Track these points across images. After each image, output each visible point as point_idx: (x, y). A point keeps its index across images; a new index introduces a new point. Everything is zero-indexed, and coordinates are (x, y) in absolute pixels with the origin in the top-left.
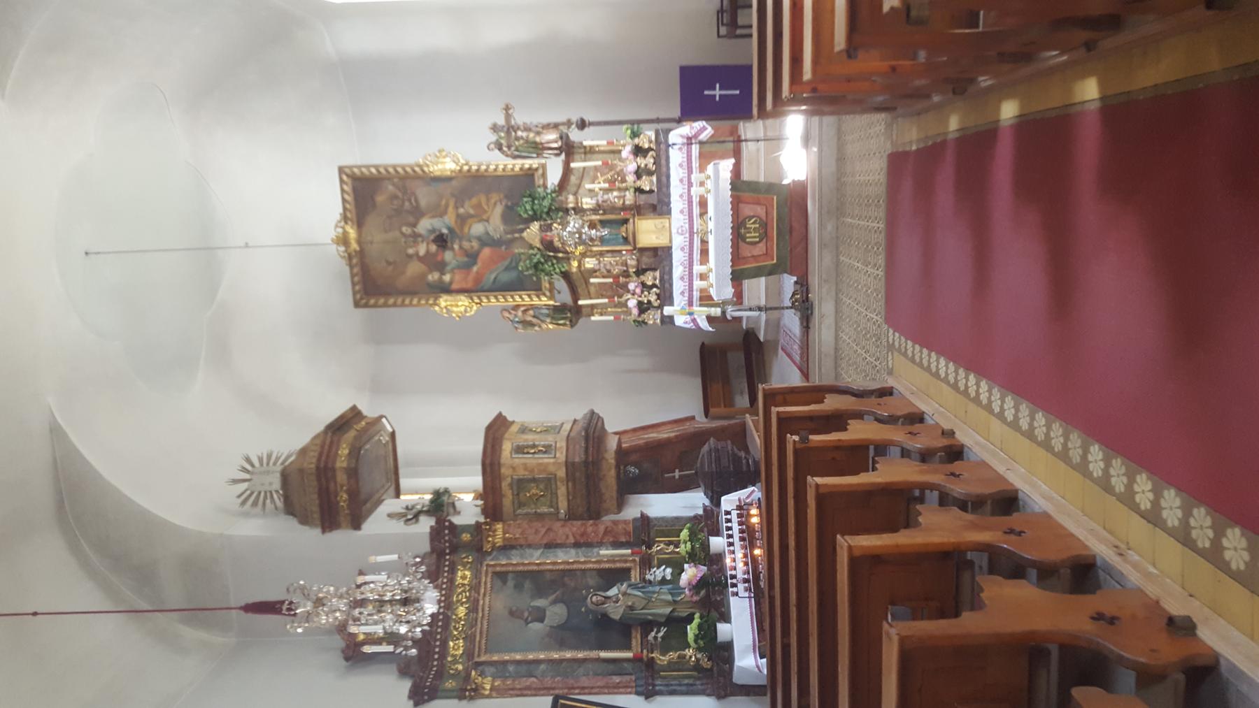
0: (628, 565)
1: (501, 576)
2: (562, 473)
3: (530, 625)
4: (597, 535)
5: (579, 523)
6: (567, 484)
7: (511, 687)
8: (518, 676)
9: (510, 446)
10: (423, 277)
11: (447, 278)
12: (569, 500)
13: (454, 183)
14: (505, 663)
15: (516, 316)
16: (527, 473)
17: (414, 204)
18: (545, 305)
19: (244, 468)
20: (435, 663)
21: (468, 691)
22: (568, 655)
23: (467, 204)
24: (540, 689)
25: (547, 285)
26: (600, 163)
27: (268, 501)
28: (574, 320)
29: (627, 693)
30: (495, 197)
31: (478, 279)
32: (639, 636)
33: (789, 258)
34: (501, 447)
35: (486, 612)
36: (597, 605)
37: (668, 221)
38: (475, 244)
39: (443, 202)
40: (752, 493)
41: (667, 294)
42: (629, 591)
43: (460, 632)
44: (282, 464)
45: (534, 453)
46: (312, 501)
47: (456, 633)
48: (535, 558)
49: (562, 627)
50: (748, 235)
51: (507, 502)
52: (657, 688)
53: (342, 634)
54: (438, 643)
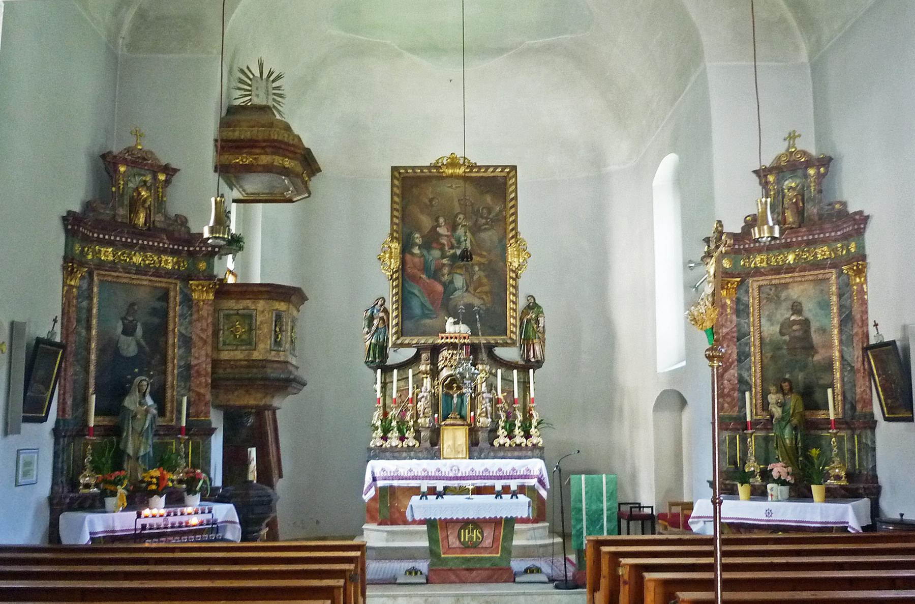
0: (168, 414)
1: (165, 296)
2: (256, 355)
3: (120, 322)
4: (197, 387)
5: (209, 370)
6: (244, 360)
8: (79, 309)
9: (282, 309)
10: (419, 230)
11: (416, 251)
12: (230, 361)
13: (501, 264)
14: (90, 299)
15: (378, 311)
16: (258, 323)
18: (388, 339)
19: (273, 73)
20: (96, 235)
21: (71, 264)
22: (93, 357)
23: (482, 274)
24: (67, 330)
25: (407, 342)
26: (516, 396)
27: (243, 93)
28: (372, 365)
31: (416, 279)
32: (106, 423)
33: (445, 568)
34: (283, 301)
35: (135, 282)
36: (138, 385)
37: (464, 456)
38: (446, 278)
39: (484, 253)
40: (233, 534)
41: (396, 454)
42: (149, 417)
43: (119, 257)
44: (274, 106)
45: (276, 331)
46: (243, 133)
47: (119, 253)
48: (176, 327)
50: (467, 531)
51: (231, 304)
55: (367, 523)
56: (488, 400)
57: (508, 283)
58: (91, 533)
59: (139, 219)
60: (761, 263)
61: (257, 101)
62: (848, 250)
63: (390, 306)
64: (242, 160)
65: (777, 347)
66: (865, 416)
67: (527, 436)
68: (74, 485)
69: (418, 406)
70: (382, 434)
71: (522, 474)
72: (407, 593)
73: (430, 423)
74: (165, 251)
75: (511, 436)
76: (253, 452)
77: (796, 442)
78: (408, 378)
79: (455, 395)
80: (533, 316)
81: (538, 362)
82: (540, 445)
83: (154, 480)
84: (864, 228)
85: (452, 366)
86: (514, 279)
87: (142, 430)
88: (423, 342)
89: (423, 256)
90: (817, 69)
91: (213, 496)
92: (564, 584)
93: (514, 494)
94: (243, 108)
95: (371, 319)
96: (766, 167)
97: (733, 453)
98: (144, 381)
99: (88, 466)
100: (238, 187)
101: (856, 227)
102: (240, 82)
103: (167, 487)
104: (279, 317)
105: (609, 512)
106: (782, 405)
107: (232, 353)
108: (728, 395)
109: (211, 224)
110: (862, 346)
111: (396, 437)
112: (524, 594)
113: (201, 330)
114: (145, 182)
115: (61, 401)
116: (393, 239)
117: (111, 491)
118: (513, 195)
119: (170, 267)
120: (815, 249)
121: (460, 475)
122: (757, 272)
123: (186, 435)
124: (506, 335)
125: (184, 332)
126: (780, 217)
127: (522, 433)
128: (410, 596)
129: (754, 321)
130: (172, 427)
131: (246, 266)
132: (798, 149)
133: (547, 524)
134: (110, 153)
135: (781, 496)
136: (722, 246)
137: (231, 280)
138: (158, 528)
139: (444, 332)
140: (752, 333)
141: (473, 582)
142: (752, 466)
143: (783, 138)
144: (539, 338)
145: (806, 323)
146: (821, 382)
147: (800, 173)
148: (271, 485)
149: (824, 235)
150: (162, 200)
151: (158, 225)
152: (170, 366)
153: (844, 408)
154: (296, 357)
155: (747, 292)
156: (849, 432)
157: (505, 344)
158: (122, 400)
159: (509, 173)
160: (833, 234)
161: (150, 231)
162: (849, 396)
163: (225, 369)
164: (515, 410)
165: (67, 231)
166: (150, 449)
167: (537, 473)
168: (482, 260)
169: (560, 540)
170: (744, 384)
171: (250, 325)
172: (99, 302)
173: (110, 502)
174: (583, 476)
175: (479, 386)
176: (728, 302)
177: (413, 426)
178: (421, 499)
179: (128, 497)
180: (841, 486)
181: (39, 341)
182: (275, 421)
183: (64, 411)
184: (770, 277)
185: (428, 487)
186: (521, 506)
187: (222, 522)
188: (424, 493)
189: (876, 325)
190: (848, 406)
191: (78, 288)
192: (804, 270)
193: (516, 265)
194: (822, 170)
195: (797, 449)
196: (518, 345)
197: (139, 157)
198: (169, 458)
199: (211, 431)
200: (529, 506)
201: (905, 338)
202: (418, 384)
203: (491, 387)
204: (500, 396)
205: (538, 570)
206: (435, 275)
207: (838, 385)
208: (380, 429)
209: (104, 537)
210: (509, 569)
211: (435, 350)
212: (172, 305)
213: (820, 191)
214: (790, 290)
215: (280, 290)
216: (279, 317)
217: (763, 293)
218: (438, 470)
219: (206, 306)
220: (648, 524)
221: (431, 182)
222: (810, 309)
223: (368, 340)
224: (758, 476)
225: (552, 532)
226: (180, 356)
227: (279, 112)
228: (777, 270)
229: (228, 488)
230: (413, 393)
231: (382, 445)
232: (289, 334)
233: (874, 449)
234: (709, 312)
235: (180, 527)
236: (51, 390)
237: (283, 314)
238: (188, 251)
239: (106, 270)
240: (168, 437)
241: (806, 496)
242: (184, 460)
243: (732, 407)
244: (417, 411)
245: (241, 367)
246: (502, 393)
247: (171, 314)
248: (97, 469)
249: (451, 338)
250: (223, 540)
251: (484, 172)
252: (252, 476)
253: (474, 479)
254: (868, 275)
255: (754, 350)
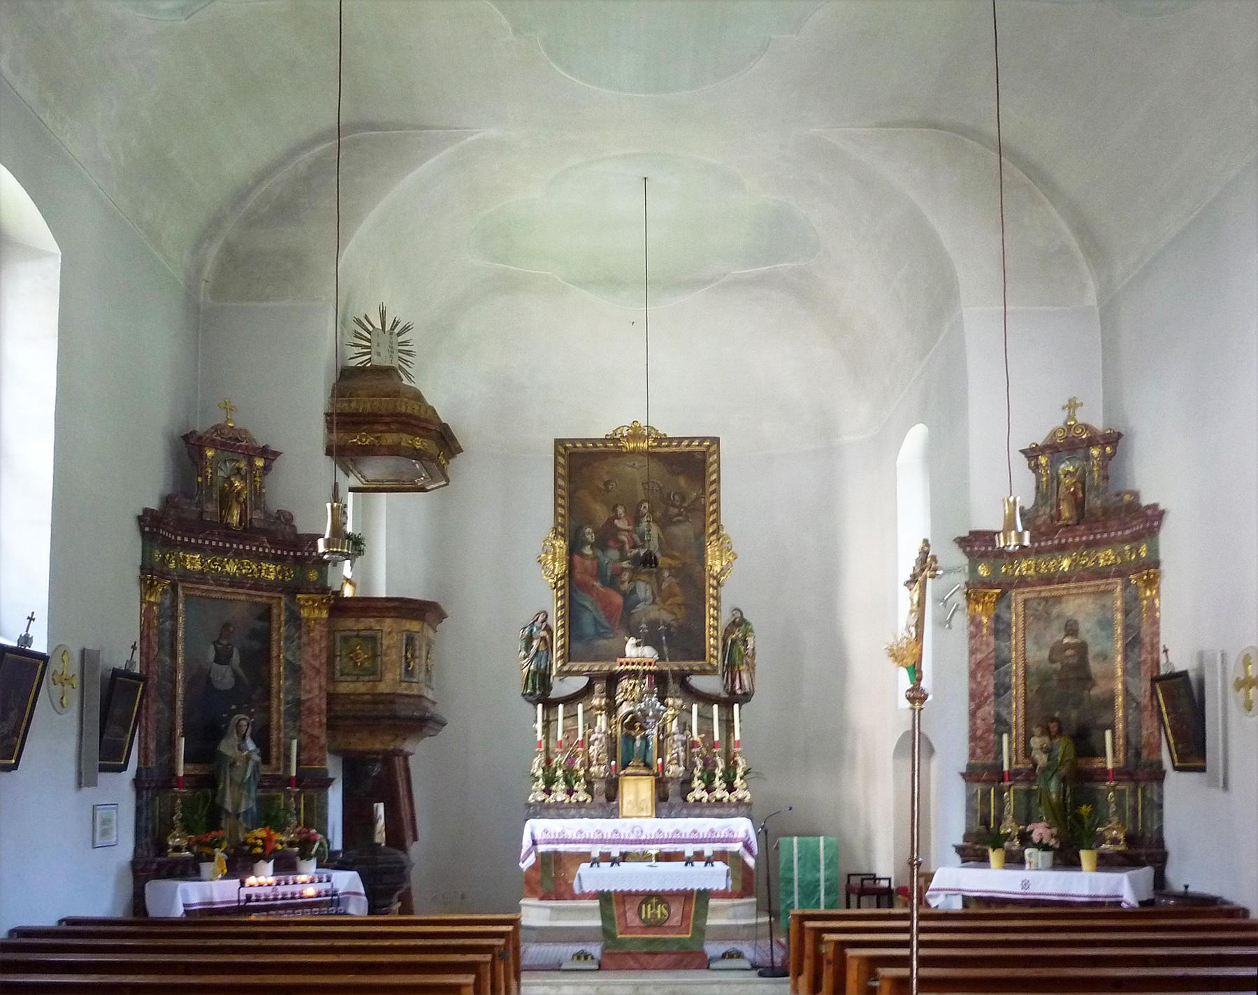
0: (274, 762)
1: (266, 614)
2: (383, 688)
3: (212, 647)
5: (324, 706)
7: (152, 626)
8: (161, 632)
9: (415, 630)
10: (590, 522)
11: (588, 551)
14: (174, 617)
16: (384, 647)
17: (675, 519)
18: (551, 665)
19: (398, 323)
20: (179, 538)
21: (150, 574)
22: (180, 690)
25: (575, 669)
26: (717, 738)
28: (531, 698)
29: (139, 757)
30: (680, 613)
32: (197, 772)
35: (229, 597)
37: (649, 814)
38: (626, 587)
39: (677, 554)
40: (358, 908)
46: (363, 404)
48: (281, 653)
49: (209, 681)
50: (649, 906)
51: (350, 624)
52: (145, 792)
53: (213, 430)
54: (200, 542)
55: (526, 897)
56: (680, 743)
57: (707, 592)
58: (185, 905)
59: (232, 517)
60: (1027, 570)
61: (378, 361)
62: (1138, 555)
63: (554, 623)
64: (360, 440)
65: (1045, 678)
66: (1151, 765)
67: (731, 789)
68: (161, 847)
69: (591, 750)
70: (544, 787)
71: (722, 836)
72: (574, 981)
73: (605, 773)
74: (266, 558)
75: (709, 789)
76: (380, 809)
77: (1064, 796)
78: (577, 715)
79: (638, 737)
80: (740, 635)
81: (745, 694)
82: (747, 800)
83: (260, 842)
84: (1159, 527)
85: (633, 700)
86: (715, 588)
87: (242, 780)
88: (596, 669)
89: (596, 557)
90: (1108, 313)
91: (331, 862)
92: (769, 971)
93: (709, 861)
94: (361, 371)
95: (529, 640)
96: (1037, 445)
97: (986, 811)
98: (242, 719)
99: (179, 824)
100: (356, 472)
101: (1148, 525)
102: (356, 337)
103: (276, 850)
104: (410, 641)
105: (828, 883)
106: (1048, 751)
107: (352, 686)
108: (981, 738)
109: (327, 536)
110: (1152, 676)
111: (562, 790)
112: (719, 983)
113: (312, 656)
114: (239, 470)
115: (142, 746)
116: (557, 534)
117: (208, 855)
118: (714, 477)
119: (272, 577)
120: (1096, 552)
121: (643, 837)
122: (1023, 582)
123: (297, 786)
124: (704, 659)
125: (291, 659)
126: (1054, 511)
127: (724, 786)
128: (578, 985)
129: (1016, 644)
130: (278, 778)
131: (366, 576)
132: (1080, 421)
133: (754, 900)
134: (194, 432)
135: (1043, 864)
136: (927, 569)
137: (348, 592)
138: (266, 900)
139: (624, 656)
140: (1013, 660)
141: (657, 968)
142: (1008, 827)
143: (1060, 407)
144: (747, 664)
145: (1082, 648)
146: (1100, 722)
147: (1081, 453)
148: (404, 849)
149: (1109, 535)
150: (261, 493)
151: (256, 524)
152: (275, 702)
153: (1126, 754)
154: (433, 689)
155: (1009, 607)
156: (1132, 785)
157: (703, 672)
158: (218, 744)
159: (708, 447)
160: (1120, 533)
161: (247, 532)
162: (1133, 740)
163: (343, 705)
164: (715, 756)
165: (143, 534)
166: (252, 804)
167: (741, 835)
168: (673, 563)
169: (766, 919)
170: (1001, 724)
171: (374, 649)
172: (186, 623)
173: (206, 868)
174: (795, 839)
175: (668, 725)
176: (985, 620)
177: (584, 776)
178: (591, 866)
179: (227, 862)
180: (1119, 853)
181: (116, 672)
182: (407, 770)
183: (146, 757)
184: (1038, 588)
185: (600, 853)
186: (716, 877)
187: (343, 894)
188: (595, 859)
189: (1166, 651)
190: (1131, 752)
191: (159, 605)
192: (1081, 579)
193: (717, 569)
194: (1108, 449)
195: (1065, 804)
196: (720, 672)
197: (230, 438)
198: (276, 816)
199: (328, 782)
200: (727, 876)
201: (1200, 670)
202: (590, 723)
203: (685, 727)
204: (696, 737)
205: (739, 955)
206: (612, 582)
207: (1120, 726)
208: (541, 780)
209: (200, 910)
210: (702, 954)
211: (612, 680)
212: (275, 625)
213: (1106, 478)
214: (1064, 605)
215: (411, 606)
216: (410, 641)
217: (1029, 608)
218: (616, 832)
219: (317, 627)
220: (885, 899)
221: (607, 459)
222: (1088, 629)
223: (527, 667)
224: (1016, 839)
225: (759, 911)
226: (287, 689)
227: (407, 374)
228: (1048, 580)
229: (350, 852)
230: (584, 735)
231: (544, 800)
232: (423, 661)
233: (1161, 806)
234: (911, 646)
235: (293, 898)
236: (130, 733)
237: (416, 636)
238: (295, 555)
239: (193, 583)
240: (274, 790)
241: (1074, 864)
242: (295, 818)
243: (986, 752)
244: (589, 758)
245: (364, 703)
246: (699, 732)
247: (275, 636)
248: (188, 828)
249: (633, 664)
250: (345, 914)
251: (676, 446)
252: (380, 837)
253: (661, 843)
254: (1162, 586)
255: (1017, 681)
